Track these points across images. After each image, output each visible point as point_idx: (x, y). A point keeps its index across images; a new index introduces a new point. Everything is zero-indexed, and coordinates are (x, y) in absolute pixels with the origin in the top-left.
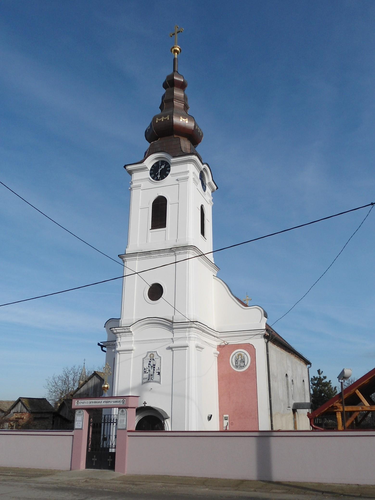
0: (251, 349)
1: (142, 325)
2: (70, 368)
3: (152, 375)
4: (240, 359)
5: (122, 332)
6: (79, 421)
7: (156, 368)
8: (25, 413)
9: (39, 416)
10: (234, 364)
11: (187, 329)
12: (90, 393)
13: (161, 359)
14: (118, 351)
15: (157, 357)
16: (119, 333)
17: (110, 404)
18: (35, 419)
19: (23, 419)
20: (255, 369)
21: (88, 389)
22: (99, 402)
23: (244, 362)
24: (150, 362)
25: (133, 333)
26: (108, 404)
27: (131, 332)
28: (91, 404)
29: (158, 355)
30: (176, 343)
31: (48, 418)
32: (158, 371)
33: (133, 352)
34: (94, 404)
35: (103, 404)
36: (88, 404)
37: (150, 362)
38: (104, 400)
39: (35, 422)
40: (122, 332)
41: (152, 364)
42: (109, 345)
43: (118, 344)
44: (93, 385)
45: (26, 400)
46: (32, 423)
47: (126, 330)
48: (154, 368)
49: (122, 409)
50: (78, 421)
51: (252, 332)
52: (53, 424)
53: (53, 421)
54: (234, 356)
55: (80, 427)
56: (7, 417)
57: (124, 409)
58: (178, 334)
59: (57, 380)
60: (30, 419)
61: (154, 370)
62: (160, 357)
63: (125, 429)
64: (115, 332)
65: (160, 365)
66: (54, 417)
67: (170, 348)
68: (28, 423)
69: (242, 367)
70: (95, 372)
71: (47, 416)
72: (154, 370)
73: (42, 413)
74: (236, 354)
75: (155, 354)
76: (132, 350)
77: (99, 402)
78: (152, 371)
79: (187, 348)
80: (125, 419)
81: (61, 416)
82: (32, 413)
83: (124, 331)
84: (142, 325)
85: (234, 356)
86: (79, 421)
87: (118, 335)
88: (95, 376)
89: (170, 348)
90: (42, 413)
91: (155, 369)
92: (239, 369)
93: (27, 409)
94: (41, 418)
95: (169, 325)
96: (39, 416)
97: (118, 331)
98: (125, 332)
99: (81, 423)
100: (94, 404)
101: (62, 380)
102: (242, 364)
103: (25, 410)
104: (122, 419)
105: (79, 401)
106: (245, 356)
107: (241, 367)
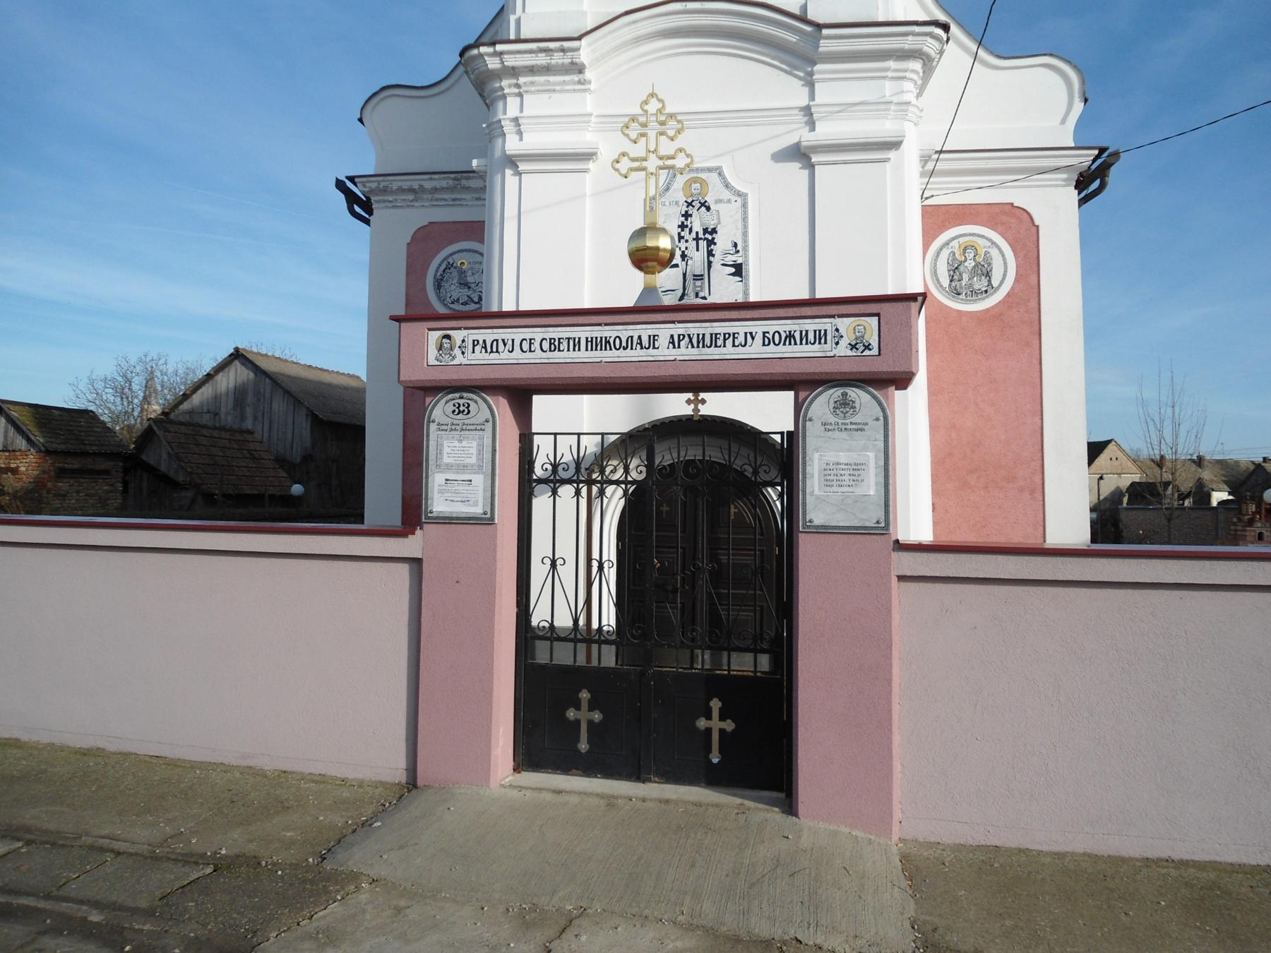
0: (1019, 227)
1: (638, 40)
2: (133, 360)
3: (698, 277)
4: (970, 264)
5: (532, 70)
6: (463, 468)
7: (723, 243)
8: (25, 454)
9: (75, 464)
10: (945, 282)
11: (892, 64)
12: (223, 409)
13: (745, 205)
14: (512, 162)
15: (726, 194)
16: (514, 72)
17: (729, 351)
18: (62, 473)
19: (15, 471)
20: (1033, 303)
21: (216, 398)
22: (629, 344)
23: (988, 275)
24: (687, 215)
25: (588, 74)
26: (713, 353)
27: (580, 69)
28: (557, 356)
29: (727, 186)
30: (827, 131)
31: (107, 472)
32: (730, 259)
33: (591, 165)
34: (584, 355)
35: (664, 352)
36: (538, 356)
37: (687, 215)
38: (678, 329)
39: (63, 485)
40: (532, 70)
41: (697, 227)
42: (385, 191)
43: (508, 127)
44: (232, 385)
45: (26, 410)
46: (49, 485)
47: (558, 59)
48: (711, 242)
49: (836, 393)
50: (449, 467)
51: (1025, 160)
52: (125, 491)
53: (126, 484)
54: (945, 253)
55: (477, 510)
56: (328, 866)
57: (853, 393)
58: (833, 88)
59: (100, 385)
60: (44, 472)
61: (710, 253)
62: (739, 194)
63: (883, 528)
64: (493, 63)
65: (745, 234)
66: (126, 471)
67: (800, 154)
68: (39, 484)
69: (975, 294)
70: (237, 349)
71: (103, 465)
72: (710, 253)
73: (84, 454)
74: (955, 243)
75: (713, 178)
76: (589, 156)
77: (629, 344)
78: (698, 258)
79: (892, 154)
80: (872, 459)
81: (151, 470)
82: (48, 452)
83: (542, 60)
84: (638, 40)
85: (945, 253)
86: (463, 468)
87: (505, 83)
88: (237, 362)
89: (800, 154)
90: (84, 454)
91: (717, 249)
92: (966, 302)
93: (29, 440)
94: (72, 473)
95: (792, 38)
96: (75, 464)
97: (510, 61)
98: (547, 70)
99: (479, 480)
100: (584, 355)
101: (115, 388)
102: (980, 284)
103: (21, 443)
104: (843, 457)
105: (458, 336)
106: (994, 253)
107: (974, 293)
